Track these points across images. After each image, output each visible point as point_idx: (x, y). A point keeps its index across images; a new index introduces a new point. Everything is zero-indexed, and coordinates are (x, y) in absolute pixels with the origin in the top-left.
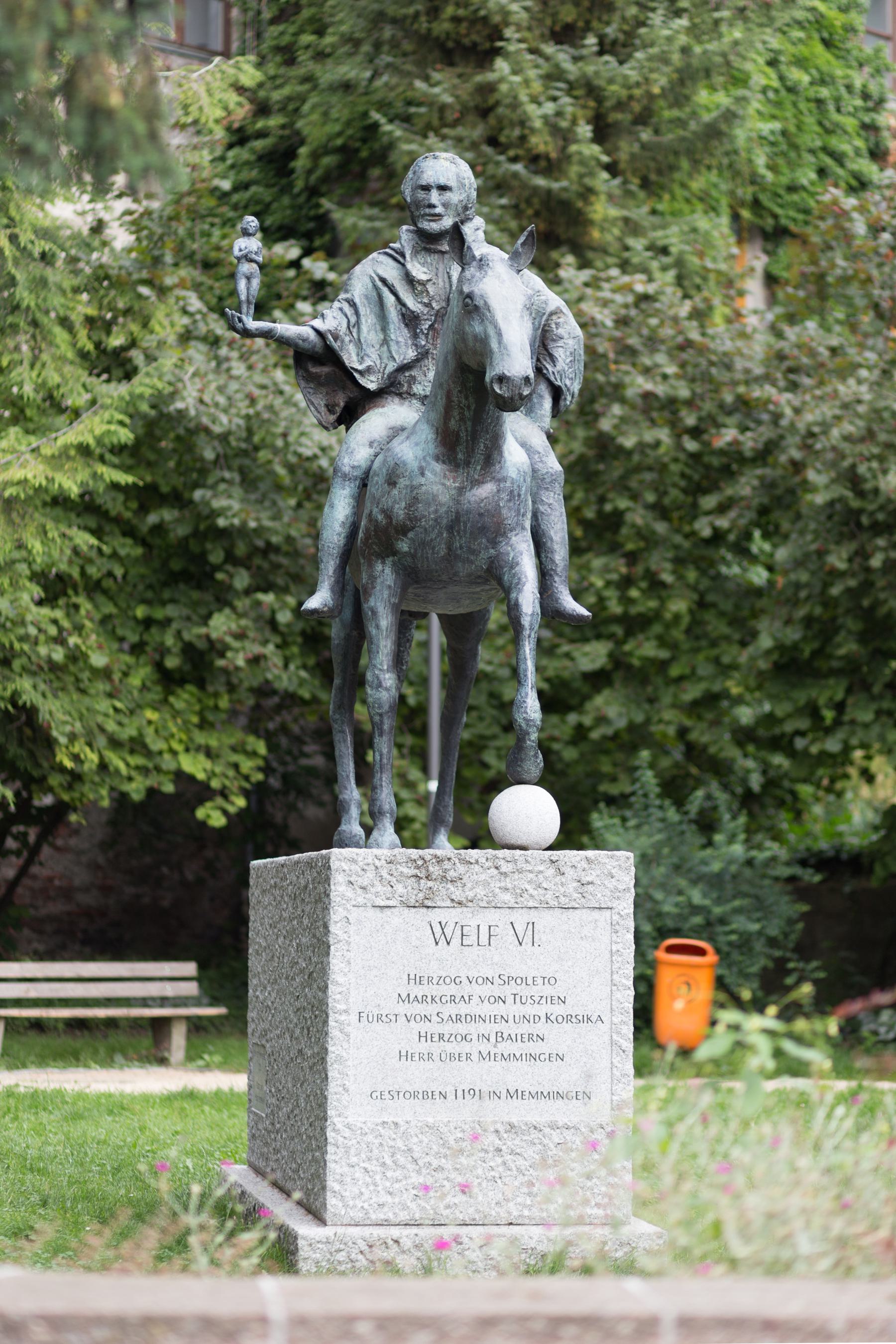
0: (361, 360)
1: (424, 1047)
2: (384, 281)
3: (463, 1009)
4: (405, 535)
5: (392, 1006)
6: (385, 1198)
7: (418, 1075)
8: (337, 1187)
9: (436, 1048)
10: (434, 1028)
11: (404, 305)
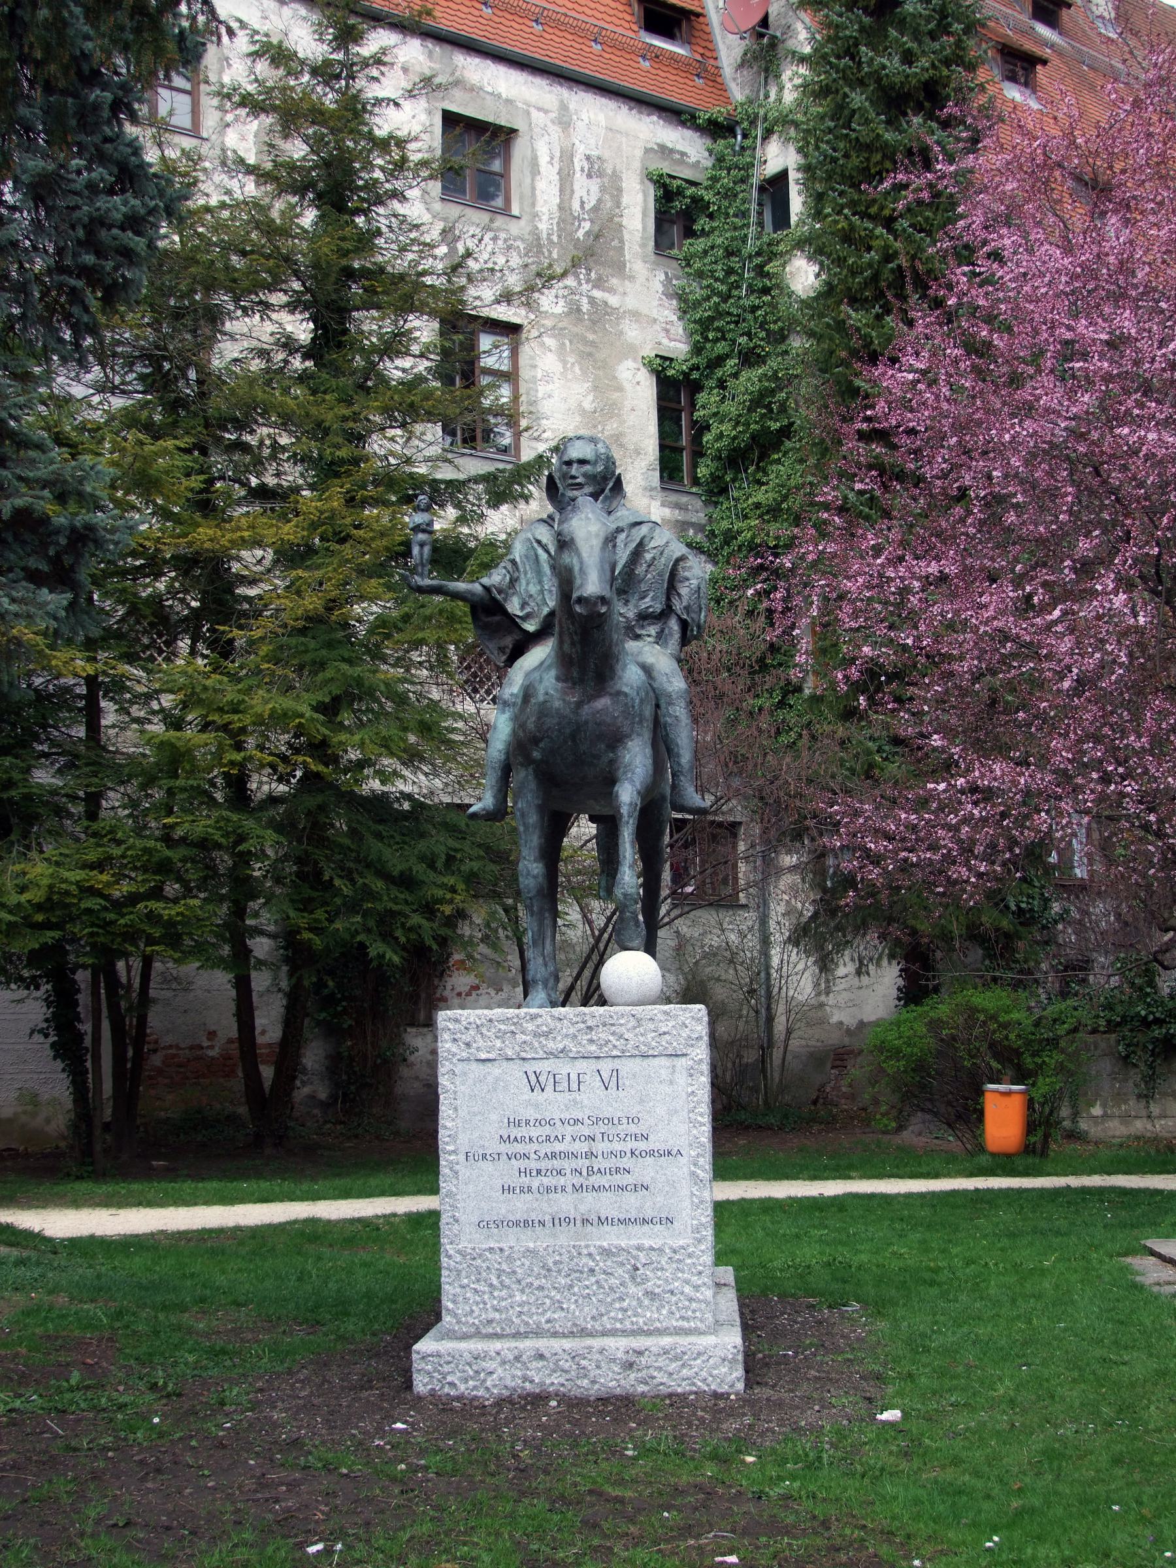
1: (525, 1180)
3: (558, 1147)
5: (494, 1147)
7: (520, 1206)
8: (450, 1305)
10: (533, 1165)
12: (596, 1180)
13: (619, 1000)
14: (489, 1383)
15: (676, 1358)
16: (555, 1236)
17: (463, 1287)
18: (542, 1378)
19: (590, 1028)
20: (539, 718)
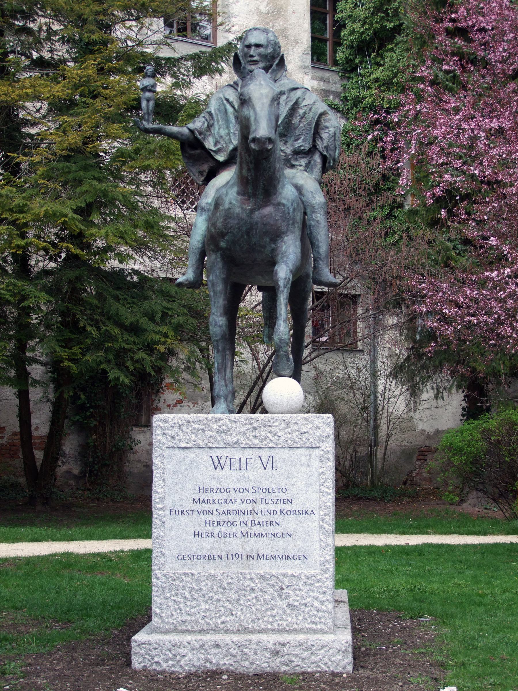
8: (158, 611)
12: (257, 529)
15: (307, 649)
16: (228, 566)
17: (166, 599)
19: (255, 428)
20: (225, 220)
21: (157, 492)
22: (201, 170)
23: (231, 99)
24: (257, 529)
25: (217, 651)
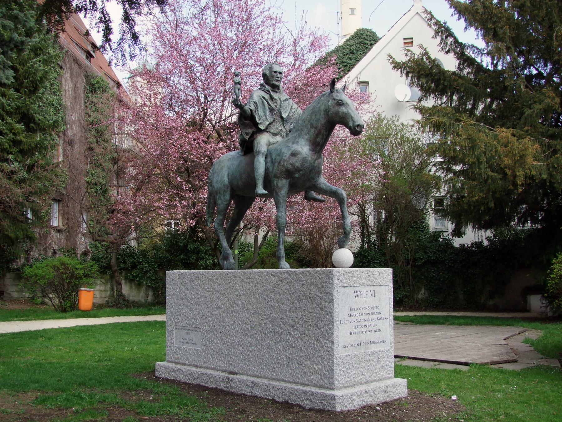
0: (259, 120)
2: (264, 98)
4: (299, 172)
6: (348, 379)
8: (337, 377)
9: (356, 330)
10: (356, 324)
11: (270, 105)
12: (370, 329)
13: (344, 266)
14: (355, 404)
15: (395, 387)
16: (361, 349)
17: (340, 370)
18: (369, 400)
19: (369, 276)
20: (303, 163)
21: (336, 311)
22: (247, 131)
23: (266, 98)
24: (370, 329)
25: (366, 394)
